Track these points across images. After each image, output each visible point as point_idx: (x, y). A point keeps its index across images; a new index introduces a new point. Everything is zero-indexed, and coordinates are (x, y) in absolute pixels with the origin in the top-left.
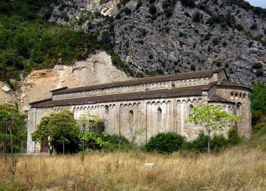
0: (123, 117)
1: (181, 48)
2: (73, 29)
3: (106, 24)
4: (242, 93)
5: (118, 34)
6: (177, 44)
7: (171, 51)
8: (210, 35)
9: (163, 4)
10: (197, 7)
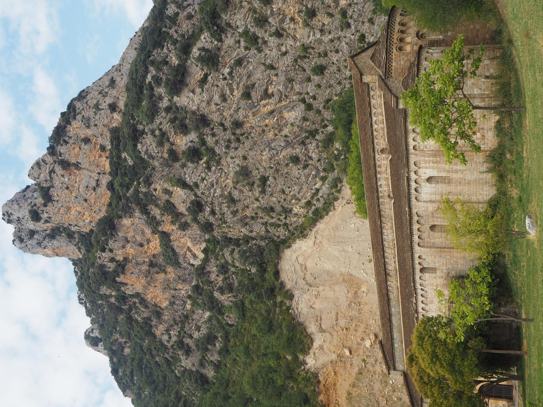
0: (442, 243)
1: (277, 97)
2: (232, 325)
3: (223, 255)
5: (246, 229)
6: (267, 104)
7: (282, 117)
8: (246, 33)
9: (181, 133)
10: (186, 60)
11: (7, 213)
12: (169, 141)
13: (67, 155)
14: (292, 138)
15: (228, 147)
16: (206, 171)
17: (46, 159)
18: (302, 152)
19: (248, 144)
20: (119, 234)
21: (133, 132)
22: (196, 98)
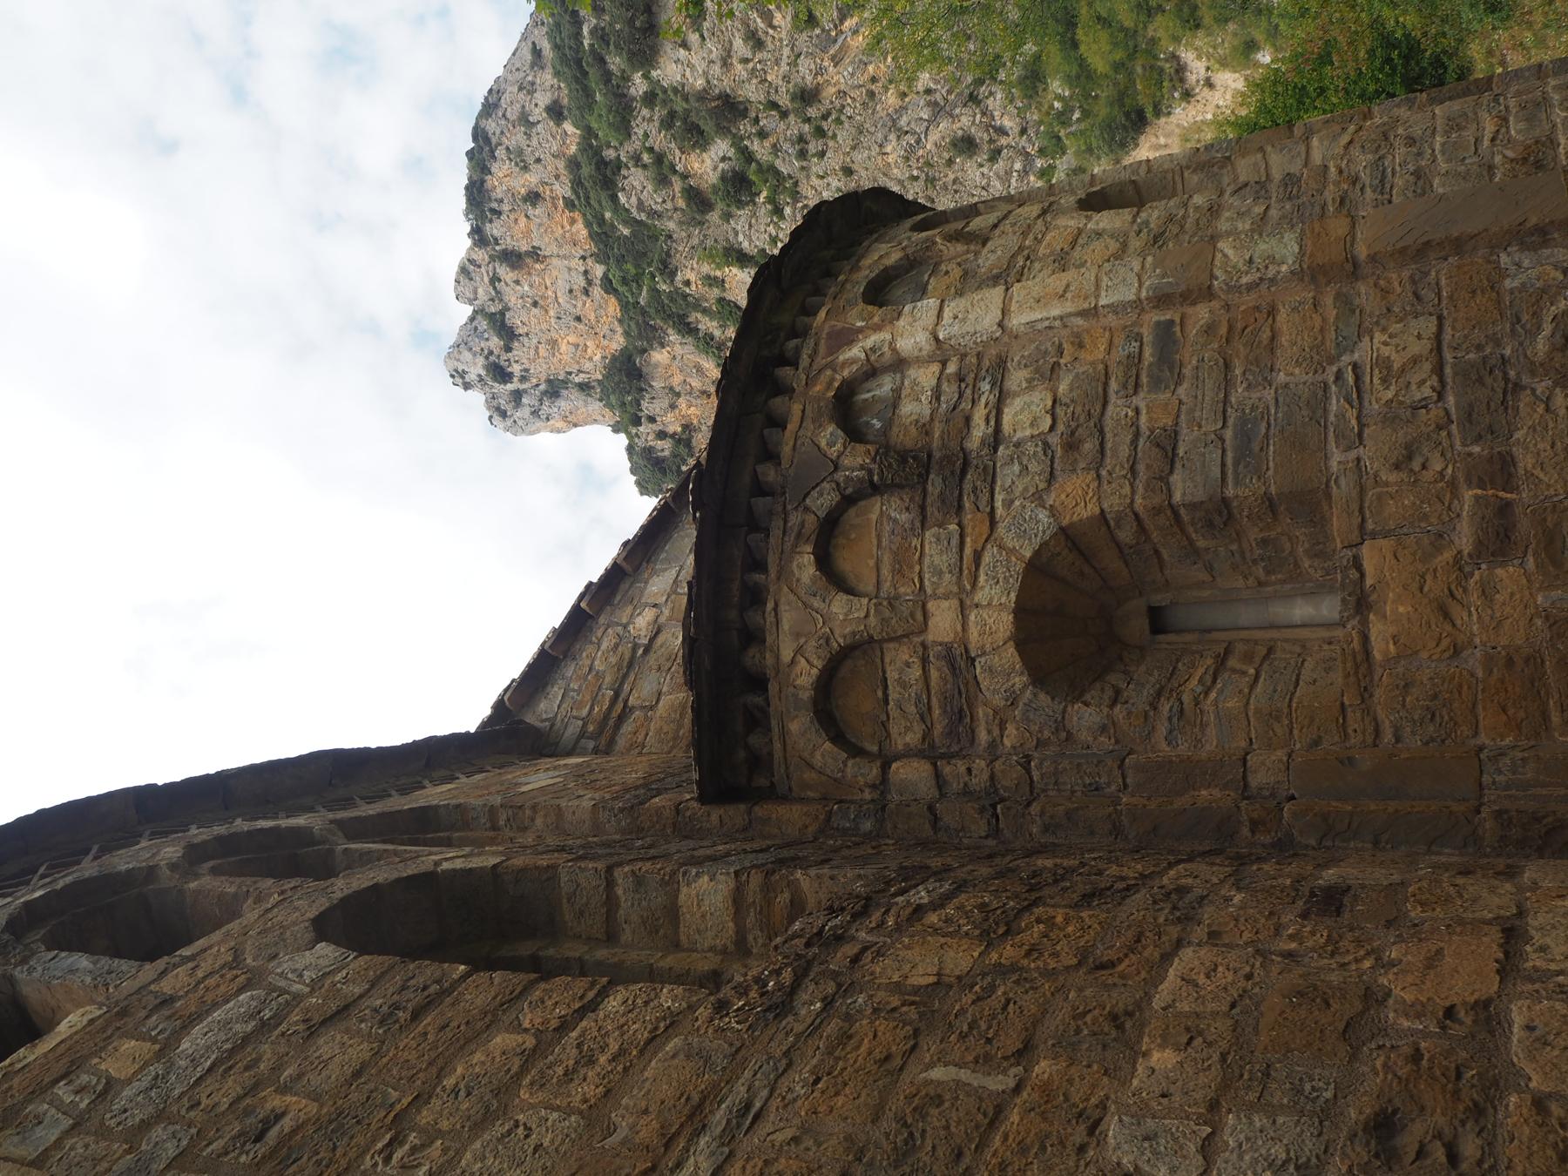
11: (456, 371)
12: (675, 172)
13: (508, 239)
14: (944, 92)
15: (802, 154)
16: (775, 219)
17: (475, 257)
18: (977, 122)
19: (844, 135)
20: (654, 384)
21: (598, 168)
22: (695, 59)
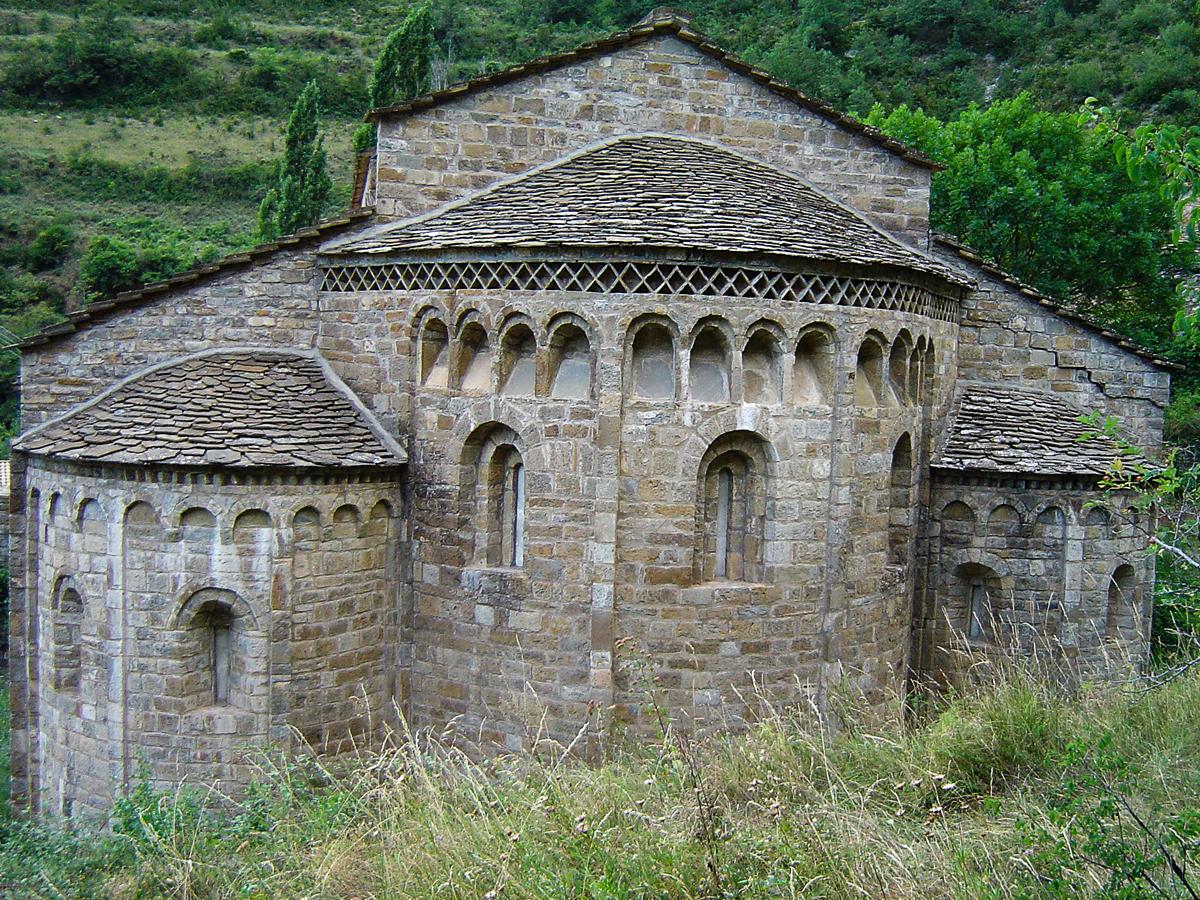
4: (771, 322)
